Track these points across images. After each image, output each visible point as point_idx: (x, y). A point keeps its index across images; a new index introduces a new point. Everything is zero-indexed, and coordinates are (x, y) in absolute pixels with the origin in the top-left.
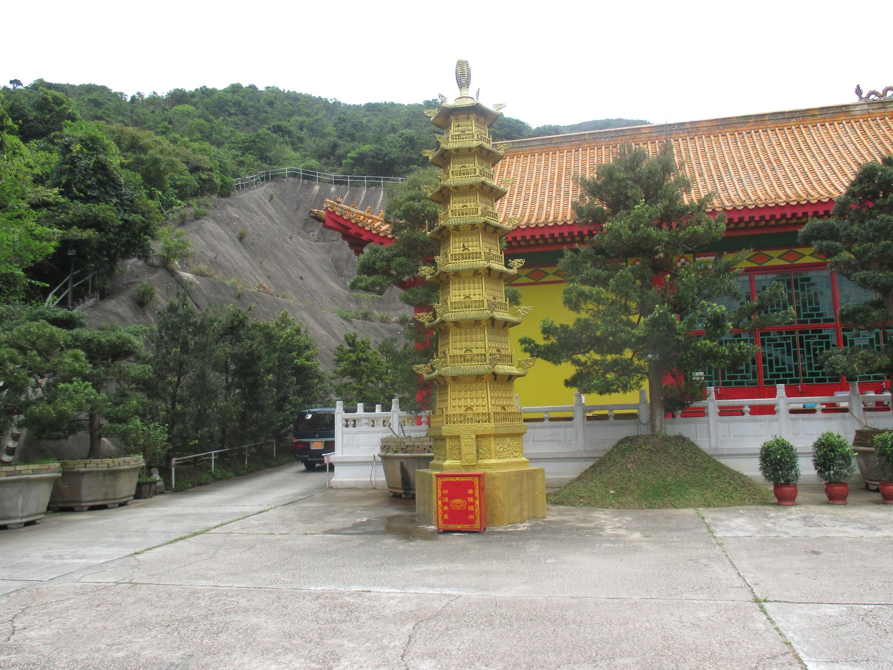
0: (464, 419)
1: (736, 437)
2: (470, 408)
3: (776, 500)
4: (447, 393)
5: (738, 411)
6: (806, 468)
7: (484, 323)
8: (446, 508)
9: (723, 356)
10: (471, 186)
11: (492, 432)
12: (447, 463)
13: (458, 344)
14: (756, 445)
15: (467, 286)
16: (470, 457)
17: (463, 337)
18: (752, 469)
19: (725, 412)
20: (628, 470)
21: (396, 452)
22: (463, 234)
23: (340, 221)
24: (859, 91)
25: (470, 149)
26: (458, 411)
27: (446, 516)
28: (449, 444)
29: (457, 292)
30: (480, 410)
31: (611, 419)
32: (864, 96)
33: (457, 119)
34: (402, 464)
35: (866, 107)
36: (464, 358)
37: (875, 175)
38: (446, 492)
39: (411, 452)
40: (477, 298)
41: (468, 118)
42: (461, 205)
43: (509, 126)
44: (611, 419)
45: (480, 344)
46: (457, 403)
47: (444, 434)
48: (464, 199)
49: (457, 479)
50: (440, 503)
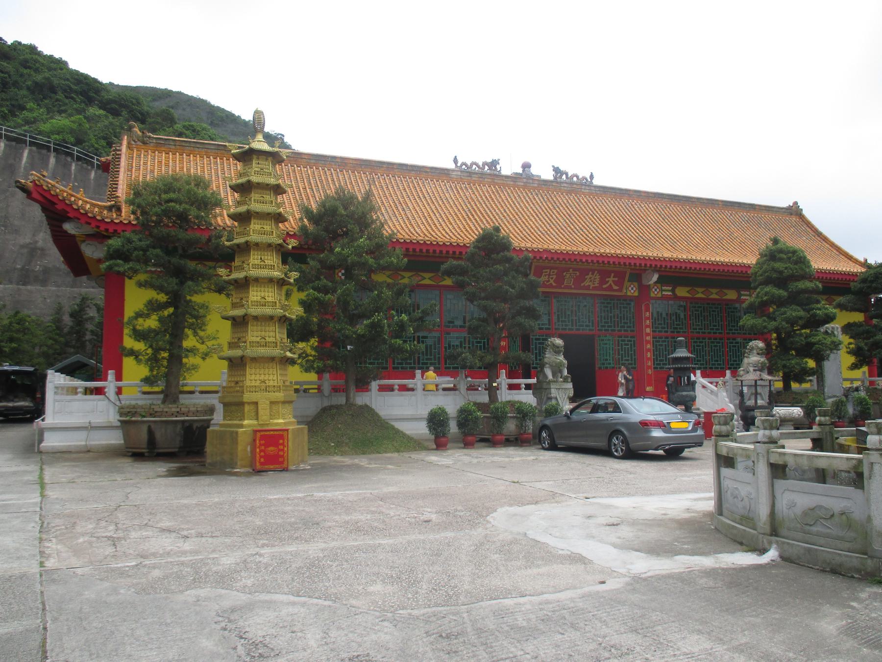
0: (256, 389)
1: (407, 405)
2: (264, 382)
3: (435, 447)
4: (245, 370)
5: (390, 388)
6: (453, 428)
7: (276, 319)
8: (262, 454)
9: (407, 351)
10: (269, 214)
11: (282, 399)
12: (246, 422)
13: (255, 333)
14: (425, 412)
15: (263, 289)
16: (265, 418)
17: (259, 328)
18: (421, 429)
19: (382, 388)
20: (339, 429)
21: (144, 417)
22: (260, 250)
23: (45, 195)
24: (455, 160)
25: (268, 185)
27: (262, 460)
28: (247, 408)
29: (255, 293)
30: (271, 383)
31: (197, 393)
32: (459, 165)
33: (258, 158)
34: (149, 427)
35: (459, 173)
36: (259, 344)
38: (263, 442)
39: (159, 417)
40: (270, 299)
41: (267, 159)
42: (260, 226)
43: (87, 84)
44: (197, 393)
45: (272, 334)
46: (253, 377)
47: (245, 400)
48: (262, 222)
50: (258, 450)
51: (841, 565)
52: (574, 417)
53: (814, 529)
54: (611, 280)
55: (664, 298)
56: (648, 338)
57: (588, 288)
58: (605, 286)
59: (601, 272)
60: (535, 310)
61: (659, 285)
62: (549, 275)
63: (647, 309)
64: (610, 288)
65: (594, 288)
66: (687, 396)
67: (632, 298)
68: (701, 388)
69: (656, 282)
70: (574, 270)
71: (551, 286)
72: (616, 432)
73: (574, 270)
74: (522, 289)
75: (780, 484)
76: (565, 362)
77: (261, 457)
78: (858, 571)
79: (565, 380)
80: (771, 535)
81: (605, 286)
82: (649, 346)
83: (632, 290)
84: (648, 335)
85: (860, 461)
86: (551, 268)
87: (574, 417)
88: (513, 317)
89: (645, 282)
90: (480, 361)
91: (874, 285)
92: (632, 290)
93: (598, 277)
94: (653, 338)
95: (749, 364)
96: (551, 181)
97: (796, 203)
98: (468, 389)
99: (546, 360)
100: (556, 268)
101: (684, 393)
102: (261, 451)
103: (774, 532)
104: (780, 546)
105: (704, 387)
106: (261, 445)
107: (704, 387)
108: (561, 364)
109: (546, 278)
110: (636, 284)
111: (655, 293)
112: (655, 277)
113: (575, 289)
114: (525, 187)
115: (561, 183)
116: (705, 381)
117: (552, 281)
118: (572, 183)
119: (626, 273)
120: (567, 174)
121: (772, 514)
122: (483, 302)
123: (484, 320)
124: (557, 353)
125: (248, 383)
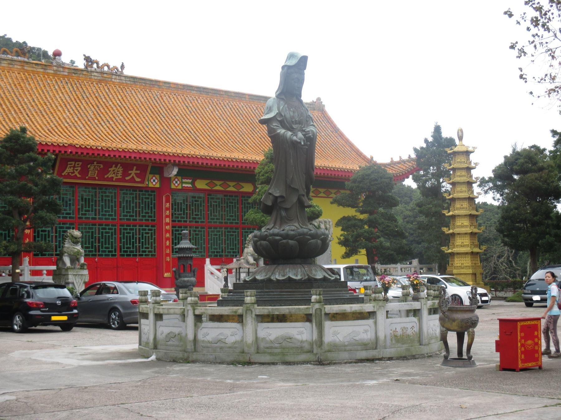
26: (458, 265)
30: (467, 264)
37: (19, 139)
38: (523, 334)
49: (529, 323)
51: (176, 358)
52: (84, 298)
53: (169, 343)
54: (133, 172)
55: (184, 190)
56: (168, 227)
57: (111, 179)
58: (127, 178)
59: (123, 165)
60: (56, 205)
61: (180, 178)
62: (74, 167)
63: (168, 201)
64: (132, 180)
65: (118, 180)
66: (188, 281)
67: (153, 189)
68: (209, 274)
69: (176, 175)
70: (99, 162)
71: (75, 177)
72: (114, 309)
73: (99, 162)
74: (45, 186)
75: (159, 323)
76: (82, 251)
77: (522, 353)
78: (182, 359)
79: (82, 267)
80: (154, 349)
81: (127, 178)
82: (168, 235)
83: (154, 182)
84: (167, 224)
85: (184, 309)
86: (76, 161)
87: (84, 298)
88: (35, 210)
89: (166, 175)
90: (4, 250)
91: (361, 185)
92: (154, 182)
93: (121, 170)
94: (173, 227)
95: (247, 253)
96: (82, 70)
97: (319, 99)
98: (430, 313)
99: (65, 249)
100: (79, 161)
101: (186, 279)
102: (522, 345)
103: (155, 347)
104: (157, 355)
105: (212, 273)
106: (522, 338)
107: (212, 273)
108: (78, 253)
109: (71, 170)
110: (158, 176)
111: (176, 185)
112: (175, 171)
113: (98, 180)
114: (55, 74)
115: (92, 72)
116: (213, 268)
117: (76, 173)
118: (103, 73)
119: (148, 166)
120: (97, 63)
121: (155, 338)
122: (10, 197)
123: (9, 213)
124: (76, 243)
125: (456, 265)
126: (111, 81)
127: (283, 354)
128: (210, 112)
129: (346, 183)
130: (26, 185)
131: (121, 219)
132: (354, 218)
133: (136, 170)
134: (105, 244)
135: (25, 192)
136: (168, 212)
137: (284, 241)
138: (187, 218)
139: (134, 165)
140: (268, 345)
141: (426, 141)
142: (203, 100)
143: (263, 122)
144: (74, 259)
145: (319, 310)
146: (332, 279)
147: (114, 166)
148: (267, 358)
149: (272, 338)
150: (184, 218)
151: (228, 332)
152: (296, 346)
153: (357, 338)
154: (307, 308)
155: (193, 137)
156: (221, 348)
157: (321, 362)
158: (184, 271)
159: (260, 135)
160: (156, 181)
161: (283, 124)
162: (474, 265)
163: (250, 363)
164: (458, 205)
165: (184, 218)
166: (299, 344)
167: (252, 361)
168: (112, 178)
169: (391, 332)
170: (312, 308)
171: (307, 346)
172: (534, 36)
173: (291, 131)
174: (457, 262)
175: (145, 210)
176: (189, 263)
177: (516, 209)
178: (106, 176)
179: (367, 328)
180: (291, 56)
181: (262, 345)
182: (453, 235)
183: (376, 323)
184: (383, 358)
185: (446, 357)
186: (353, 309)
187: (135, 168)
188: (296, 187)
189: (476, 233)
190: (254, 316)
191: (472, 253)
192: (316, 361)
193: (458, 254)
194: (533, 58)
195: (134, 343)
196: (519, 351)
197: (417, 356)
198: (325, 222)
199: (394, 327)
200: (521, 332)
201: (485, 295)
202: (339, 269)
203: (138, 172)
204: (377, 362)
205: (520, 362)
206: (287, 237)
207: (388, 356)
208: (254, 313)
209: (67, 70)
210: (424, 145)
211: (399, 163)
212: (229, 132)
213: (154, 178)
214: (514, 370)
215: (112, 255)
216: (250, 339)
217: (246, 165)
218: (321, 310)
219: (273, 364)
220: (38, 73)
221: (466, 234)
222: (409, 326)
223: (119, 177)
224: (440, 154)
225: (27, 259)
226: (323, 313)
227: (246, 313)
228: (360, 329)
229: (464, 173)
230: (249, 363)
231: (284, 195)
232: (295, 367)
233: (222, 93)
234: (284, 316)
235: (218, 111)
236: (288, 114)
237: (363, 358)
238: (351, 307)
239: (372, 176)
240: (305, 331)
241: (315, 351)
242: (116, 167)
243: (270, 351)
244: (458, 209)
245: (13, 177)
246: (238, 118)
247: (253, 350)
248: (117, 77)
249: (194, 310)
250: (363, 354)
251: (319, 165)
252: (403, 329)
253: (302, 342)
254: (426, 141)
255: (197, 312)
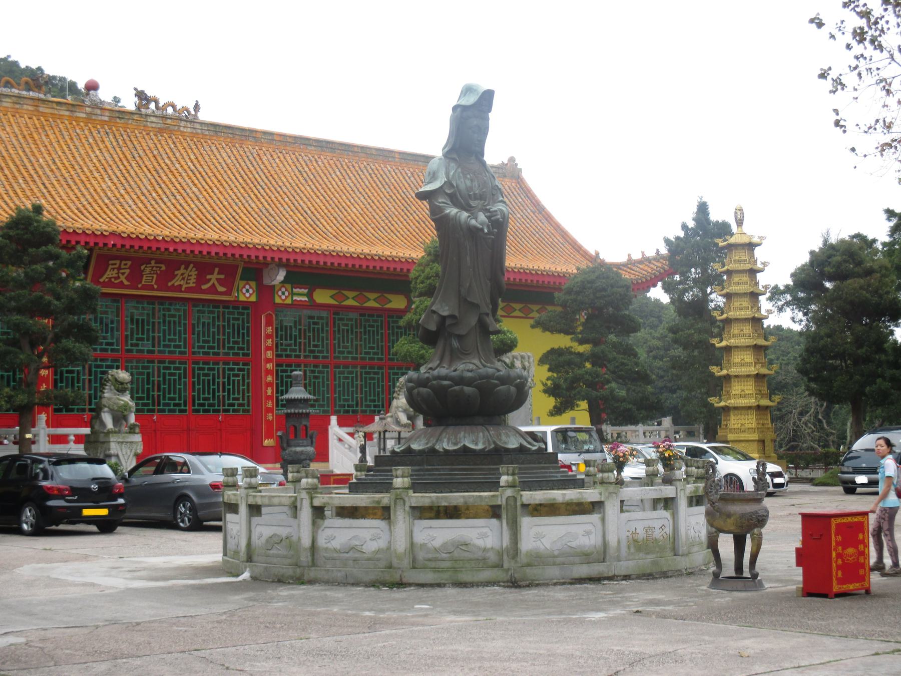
26: (736, 426)
30: (750, 426)
37: (31, 224)
38: (839, 538)
49: (849, 519)
51: (283, 576)
52: (135, 480)
53: (271, 552)
54: (214, 278)
55: (296, 305)
56: (269, 366)
57: (178, 289)
58: (204, 287)
59: (197, 265)
60: (90, 329)
61: (289, 286)
62: (119, 269)
63: (269, 323)
64: (213, 290)
65: (189, 290)
66: (302, 453)
67: (246, 305)
68: (336, 442)
69: (282, 282)
70: (158, 261)
71: (121, 285)
72: (183, 498)
73: (158, 261)
74: (72, 300)
75: (256, 520)
76: (132, 404)
77: (838, 567)
78: (292, 577)
79: (132, 430)
80: (247, 561)
81: (204, 287)
82: (269, 378)
83: (247, 293)
84: (269, 361)
85: (296, 498)
86: (122, 258)
87: (135, 480)
88: (57, 339)
89: (266, 281)
90: (7, 402)
91: (580, 298)
92: (247, 293)
93: (194, 273)
94: (277, 365)
95: (397, 407)
96: (131, 113)
97: (512, 159)
98: (690, 504)
99: (104, 401)
100: (126, 259)
101: (299, 449)
102: (839, 556)
103: (250, 559)
104: (252, 572)
105: (340, 440)
106: (838, 544)
107: (340, 440)
108: (126, 407)
109: (114, 273)
110: (253, 284)
111: (282, 297)
112: (281, 275)
113: (157, 290)
114: (89, 120)
115: (147, 115)
116: (342, 432)
117: (123, 278)
118: (165, 117)
119: (237, 266)
120: (156, 102)
121: (249, 545)
122: (16, 318)
123: (14, 343)
124: (122, 391)
125: (732, 426)
126: (179, 130)
127: (455, 570)
128: (337, 179)
129: (556, 294)
130: (41, 297)
131: (194, 353)
132: (568, 351)
133: (219, 273)
134: (169, 393)
135: (39, 309)
136: (270, 341)
137: (456, 388)
138: (300, 351)
139: (216, 265)
140: (430, 556)
141: (684, 227)
142: (325, 161)
143: (422, 196)
144: (119, 417)
145: (512, 499)
146: (534, 448)
147: (183, 267)
148: (429, 577)
149: (437, 543)
150: (295, 351)
151: (366, 534)
152: (476, 556)
153: (573, 544)
154: (493, 496)
155: (309, 220)
156: (355, 560)
157: (516, 582)
158: (296, 436)
159: (417, 218)
160: (251, 291)
161: (454, 199)
162: (761, 426)
163: (402, 584)
164: (735, 329)
165: (295, 351)
166: (480, 553)
167: (405, 580)
168: (181, 286)
169: (628, 534)
170: (502, 496)
171: (493, 558)
172: (857, 58)
173: (467, 211)
174: (734, 421)
175: (234, 337)
176: (304, 423)
177: (829, 336)
178: (170, 284)
179: (589, 527)
180: (468, 90)
181: (421, 555)
182: (728, 378)
183: (603, 520)
184: (614, 576)
185: (716, 575)
186: (567, 498)
187: (217, 270)
188: (475, 302)
189: (764, 376)
190: (407, 508)
191: (758, 407)
192: (507, 582)
193: (736, 408)
194: (855, 94)
195: (216, 552)
196: (834, 565)
197: (670, 574)
198: (523, 357)
199: (632, 526)
200: (836, 534)
201: (779, 475)
202: (545, 433)
203: (222, 277)
204: (605, 582)
205: (835, 582)
206: (460, 381)
207: (624, 573)
208: (408, 505)
209: (107, 113)
210: (682, 234)
211: (640, 262)
212: (368, 213)
213: (247, 287)
214: (825, 596)
215: (180, 411)
216: (401, 545)
217: (395, 266)
218: (515, 499)
219: (439, 585)
220: (61, 117)
221: (748, 376)
222: (657, 524)
223: (192, 285)
224: (707, 248)
225: (43, 417)
226: (519, 504)
227: (395, 504)
228: (579, 530)
229: (745, 278)
230: (400, 584)
231: (457, 314)
232: (473, 590)
233: (356, 150)
234: (456, 508)
235: (350, 179)
236: (463, 184)
237: (583, 576)
238: (564, 495)
239: (598, 284)
240: (490, 533)
241: (506, 566)
242: (186, 268)
243: (433, 564)
244: (735, 336)
245: (21, 285)
246: (383, 190)
247: (406, 563)
248: (189, 125)
249: (312, 498)
250: (583, 571)
251: (513, 265)
252: (648, 529)
253: (485, 550)
254: (684, 227)
255: (317, 503)
